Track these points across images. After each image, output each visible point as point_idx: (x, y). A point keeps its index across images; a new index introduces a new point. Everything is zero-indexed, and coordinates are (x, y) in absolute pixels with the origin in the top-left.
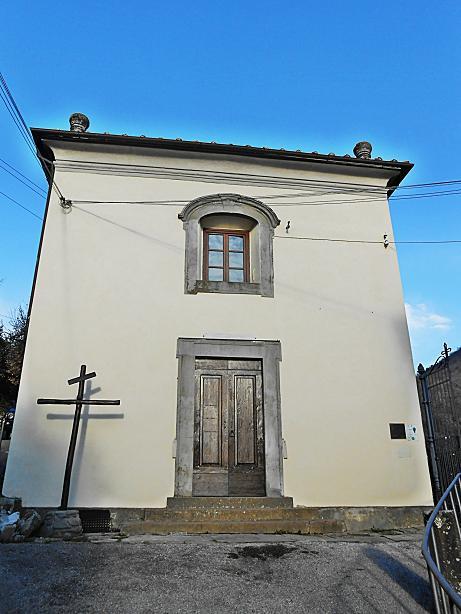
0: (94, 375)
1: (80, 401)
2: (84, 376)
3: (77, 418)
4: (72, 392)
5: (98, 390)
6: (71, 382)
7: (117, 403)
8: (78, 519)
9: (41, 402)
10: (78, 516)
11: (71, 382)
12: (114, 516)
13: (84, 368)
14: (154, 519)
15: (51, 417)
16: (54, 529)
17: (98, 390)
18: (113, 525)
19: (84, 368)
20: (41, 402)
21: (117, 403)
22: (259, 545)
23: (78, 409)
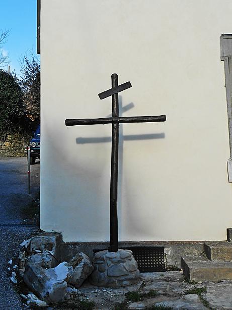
0: (127, 85)
1: (115, 120)
2: (116, 88)
3: (115, 140)
4: (105, 108)
5: (131, 106)
6: (102, 96)
7: (162, 119)
8: (134, 262)
9: (70, 123)
10: (133, 260)
11: (102, 96)
12: (168, 251)
13: (115, 77)
14: (223, 259)
15: (80, 141)
16: (109, 276)
17: (131, 106)
18: (168, 261)
19: (115, 77)
20: (70, 123)
21: (162, 119)
22: (176, 271)
23: (115, 129)
